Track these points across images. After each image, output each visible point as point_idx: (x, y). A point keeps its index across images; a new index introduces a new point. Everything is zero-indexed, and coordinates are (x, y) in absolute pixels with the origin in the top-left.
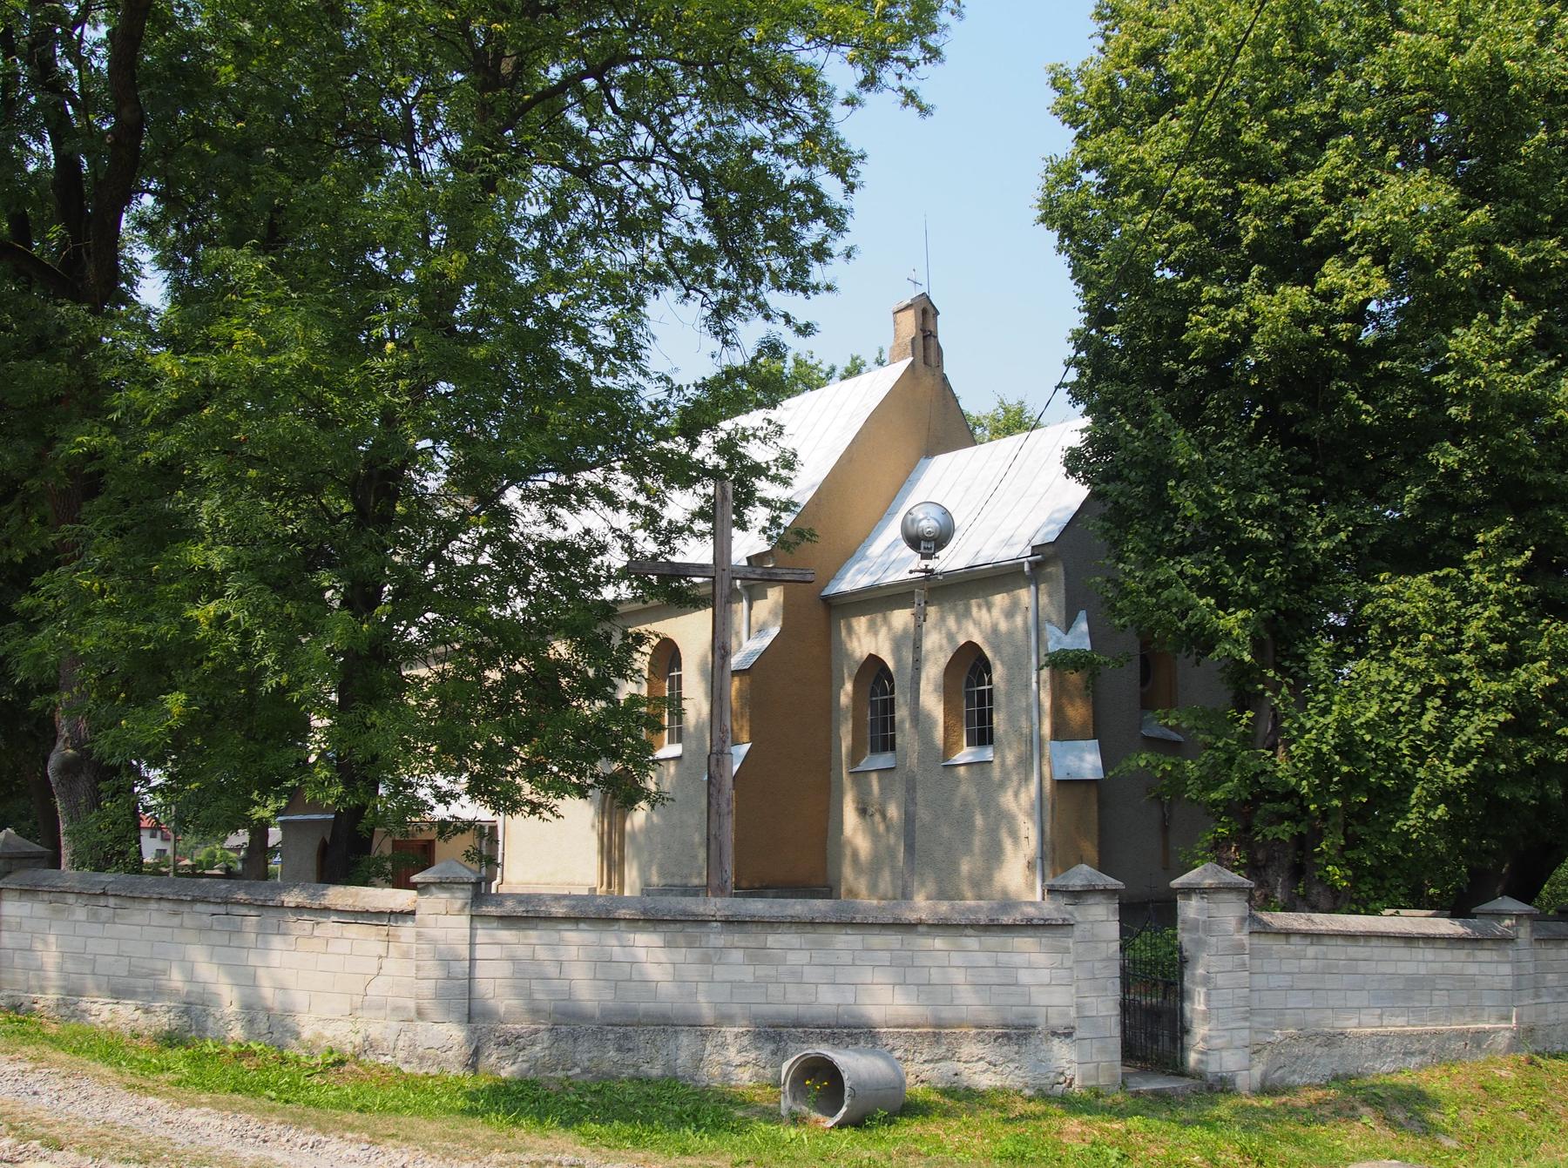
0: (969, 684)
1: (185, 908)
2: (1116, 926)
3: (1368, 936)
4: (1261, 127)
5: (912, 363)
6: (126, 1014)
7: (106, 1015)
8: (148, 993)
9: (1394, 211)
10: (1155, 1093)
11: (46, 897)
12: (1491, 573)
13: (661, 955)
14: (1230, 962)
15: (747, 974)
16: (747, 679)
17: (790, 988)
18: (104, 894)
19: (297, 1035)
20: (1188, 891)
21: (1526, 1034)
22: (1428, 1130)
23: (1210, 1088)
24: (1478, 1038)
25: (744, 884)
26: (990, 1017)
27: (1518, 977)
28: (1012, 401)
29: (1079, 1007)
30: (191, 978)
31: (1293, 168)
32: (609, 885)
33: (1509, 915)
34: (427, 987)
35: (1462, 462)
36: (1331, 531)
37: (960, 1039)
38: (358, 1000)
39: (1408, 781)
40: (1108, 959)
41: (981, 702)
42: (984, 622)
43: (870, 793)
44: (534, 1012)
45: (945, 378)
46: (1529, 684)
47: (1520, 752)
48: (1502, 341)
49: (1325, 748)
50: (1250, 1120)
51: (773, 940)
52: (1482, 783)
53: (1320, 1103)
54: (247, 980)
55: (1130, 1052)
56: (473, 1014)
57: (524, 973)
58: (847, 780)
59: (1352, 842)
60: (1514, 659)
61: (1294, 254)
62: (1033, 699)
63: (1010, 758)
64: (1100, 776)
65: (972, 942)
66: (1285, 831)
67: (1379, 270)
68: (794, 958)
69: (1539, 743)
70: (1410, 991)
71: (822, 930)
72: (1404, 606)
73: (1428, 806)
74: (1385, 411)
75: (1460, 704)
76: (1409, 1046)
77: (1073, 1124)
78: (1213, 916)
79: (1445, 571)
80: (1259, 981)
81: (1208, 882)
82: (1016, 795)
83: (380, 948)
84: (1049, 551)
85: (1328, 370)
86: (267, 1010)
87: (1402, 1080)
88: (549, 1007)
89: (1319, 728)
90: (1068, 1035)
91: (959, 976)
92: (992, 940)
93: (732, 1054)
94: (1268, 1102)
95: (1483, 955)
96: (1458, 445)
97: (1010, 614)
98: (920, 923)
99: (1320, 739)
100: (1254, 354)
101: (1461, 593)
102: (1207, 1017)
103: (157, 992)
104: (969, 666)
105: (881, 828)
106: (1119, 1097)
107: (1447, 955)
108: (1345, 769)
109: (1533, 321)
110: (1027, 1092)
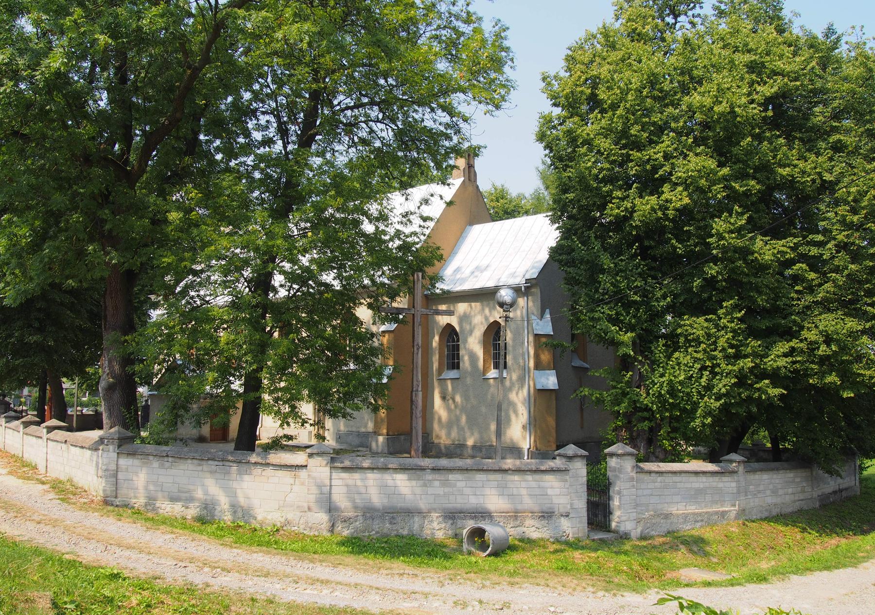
1: (204, 463)
2: (585, 471)
3: (681, 472)
4: (638, 127)
6: (174, 509)
7: (168, 509)
8: (187, 500)
9: (692, 171)
10: (600, 540)
11: (140, 457)
13: (408, 483)
14: (628, 485)
15: (440, 491)
16: (392, 335)
17: (458, 497)
19: (255, 518)
20: (612, 455)
21: (742, 512)
22: (706, 554)
23: (621, 537)
24: (723, 514)
25: (391, 433)
26: (536, 508)
27: (738, 488)
28: (499, 185)
29: (571, 504)
30: (206, 493)
31: (651, 142)
33: (735, 462)
34: (312, 498)
35: (717, 272)
36: (664, 297)
37: (524, 518)
39: (696, 405)
40: (582, 484)
43: (447, 389)
44: (356, 508)
45: (477, 187)
46: (743, 367)
47: (740, 394)
49: (663, 392)
50: (640, 551)
51: (451, 477)
52: (725, 408)
53: (664, 543)
54: (232, 494)
55: (590, 523)
56: (331, 509)
57: (351, 492)
58: (436, 383)
60: (738, 356)
61: (651, 182)
62: (525, 349)
63: (515, 377)
65: (529, 477)
66: (646, 425)
68: (459, 484)
69: (747, 389)
70: (696, 495)
71: (470, 472)
72: (695, 331)
73: (704, 417)
75: (716, 374)
76: (697, 518)
77: (577, 554)
78: (621, 463)
79: (711, 316)
80: (640, 492)
81: (620, 452)
82: (517, 394)
83: (292, 481)
84: (534, 282)
85: (662, 230)
86: (242, 507)
87: (695, 533)
88: (361, 505)
89: (660, 382)
90: (567, 516)
91: (524, 492)
92: (537, 477)
93: (435, 525)
94: (644, 543)
95: (725, 479)
96: (716, 265)
98: (510, 469)
99: (661, 386)
100: (635, 221)
101: (717, 326)
102: (619, 507)
103: (191, 499)
104: (494, 332)
105: (453, 407)
106: (588, 542)
107: (711, 479)
108: (671, 401)
109: (745, 217)
110: (552, 540)
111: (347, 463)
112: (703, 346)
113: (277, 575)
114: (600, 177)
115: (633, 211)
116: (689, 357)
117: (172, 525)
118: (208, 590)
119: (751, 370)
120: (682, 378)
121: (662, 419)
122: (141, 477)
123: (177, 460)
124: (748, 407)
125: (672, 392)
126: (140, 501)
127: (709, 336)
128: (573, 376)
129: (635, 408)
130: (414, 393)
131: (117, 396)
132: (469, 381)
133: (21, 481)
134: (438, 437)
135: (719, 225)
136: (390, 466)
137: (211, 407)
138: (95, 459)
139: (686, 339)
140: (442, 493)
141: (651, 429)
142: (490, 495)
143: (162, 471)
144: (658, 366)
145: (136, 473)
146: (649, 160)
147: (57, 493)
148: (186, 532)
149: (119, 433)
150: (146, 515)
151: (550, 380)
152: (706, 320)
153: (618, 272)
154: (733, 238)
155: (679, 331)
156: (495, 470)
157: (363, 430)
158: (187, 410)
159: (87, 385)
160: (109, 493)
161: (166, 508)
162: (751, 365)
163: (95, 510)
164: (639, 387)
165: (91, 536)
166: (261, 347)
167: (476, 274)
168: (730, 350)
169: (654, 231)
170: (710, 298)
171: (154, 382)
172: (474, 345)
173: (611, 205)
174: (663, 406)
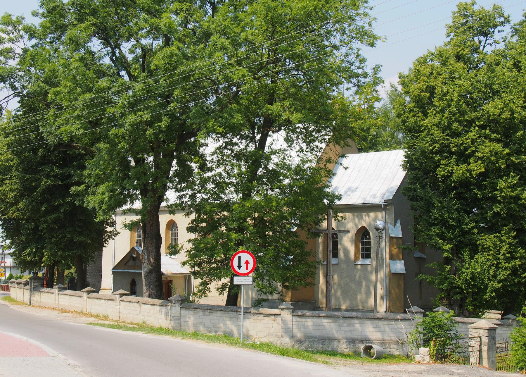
1: (227, 313)
12: (507, 237)
15: (347, 329)
25: (293, 300)
33: (511, 319)
35: (501, 210)
38: (267, 333)
39: (486, 286)
42: (367, 220)
47: (513, 280)
48: (510, 183)
49: (468, 278)
59: (475, 300)
60: (513, 258)
61: (463, 156)
64: (404, 272)
66: (458, 297)
67: (482, 165)
72: (487, 243)
74: (483, 194)
75: (500, 268)
83: (273, 322)
85: (471, 183)
89: (467, 272)
95: (504, 329)
99: (467, 274)
101: (501, 240)
104: (363, 234)
108: (472, 283)
111: (300, 313)
112: (492, 252)
114: (434, 151)
115: (452, 172)
116: (484, 258)
119: (520, 266)
120: (479, 270)
121: (468, 293)
123: (212, 311)
124: (519, 287)
125: (473, 277)
126: (191, 330)
127: (496, 246)
128: (416, 265)
129: (452, 287)
132: (344, 266)
134: (322, 303)
135: (501, 184)
136: (321, 315)
139: (483, 247)
141: (461, 299)
142: (371, 331)
144: (466, 263)
145: (190, 318)
146: (462, 144)
151: (399, 266)
152: (495, 237)
153: (443, 207)
154: (509, 192)
155: (478, 243)
156: (375, 319)
162: (519, 263)
164: (455, 274)
167: (348, 193)
168: (507, 255)
169: (465, 184)
170: (497, 223)
172: (348, 244)
173: (439, 169)
174: (468, 286)
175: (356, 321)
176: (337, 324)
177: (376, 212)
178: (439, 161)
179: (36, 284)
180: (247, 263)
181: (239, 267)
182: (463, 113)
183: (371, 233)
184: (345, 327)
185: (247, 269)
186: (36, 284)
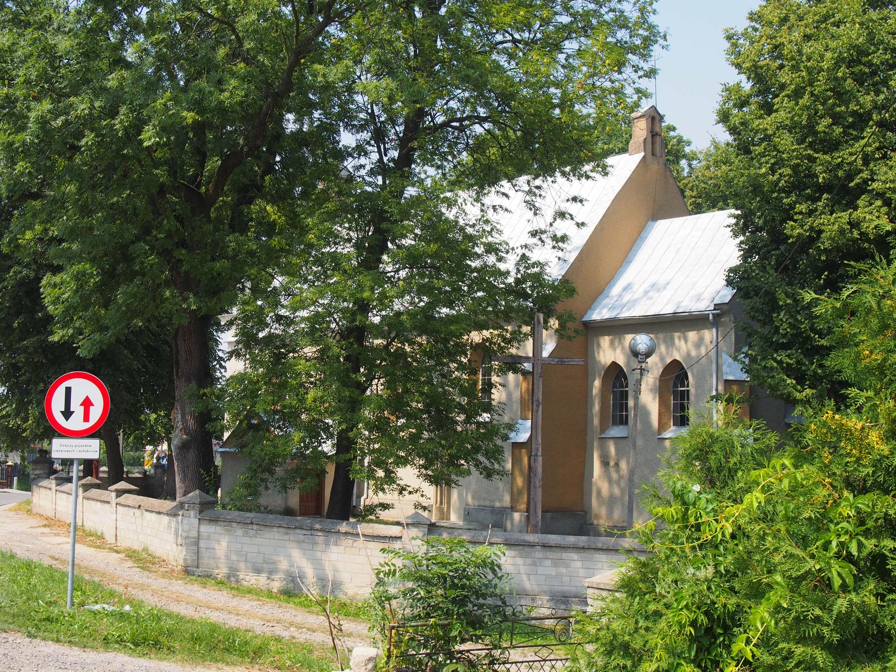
0: (675, 386)
1: (291, 531)
5: (644, 157)
6: (261, 581)
7: (253, 581)
11: (222, 523)
15: (553, 571)
18: (252, 523)
32: (441, 503)
41: (682, 398)
42: (684, 347)
51: (565, 555)
54: (318, 565)
61: (845, 193)
71: (588, 551)
84: (726, 307)
97: (699, 344)
104: (675, 376)
113: (359, 636)
117: (257, 594)
118: (294, 641)
122: (223, 544)
126: (221, 572)
130: (532, 458)
131: (192, 455)
133: (93, 549)
134: (597, 516)
137: (297, 470)
138: (173, 525)
140: (554, 573)
143: (247, 540)
145: (218, 541)
147: (134, 562)
148: (272, 600)
149: (200, 496)
150: (230, 582)
157: (497, 504)
158: (272, 473)
159: (135, 438)
160: (189, 562)
161: (250, 579)
163: (177, 579)
165: (180, 599)
166: (351, 406)
167: (650, 294)
171: (225, 438)
175: (574, 556)
176: (529, 561)
177: (699, 330)
178: (792, 206)
179: (37, 472)
180: (87, 403)
181: (67, 414)
182: (841, 96)
183: (689, 375)
184: (547, 568)
185: (86, 418)
186: (37, 472)
